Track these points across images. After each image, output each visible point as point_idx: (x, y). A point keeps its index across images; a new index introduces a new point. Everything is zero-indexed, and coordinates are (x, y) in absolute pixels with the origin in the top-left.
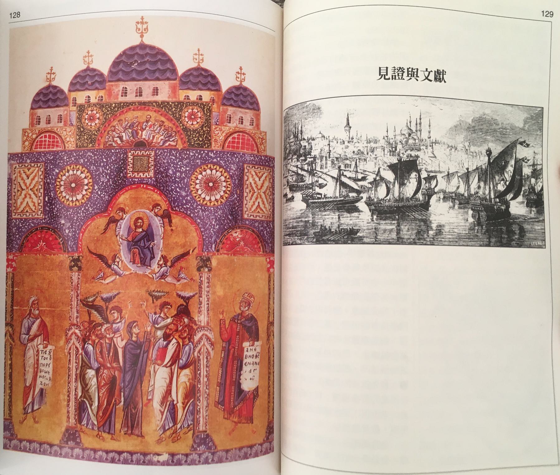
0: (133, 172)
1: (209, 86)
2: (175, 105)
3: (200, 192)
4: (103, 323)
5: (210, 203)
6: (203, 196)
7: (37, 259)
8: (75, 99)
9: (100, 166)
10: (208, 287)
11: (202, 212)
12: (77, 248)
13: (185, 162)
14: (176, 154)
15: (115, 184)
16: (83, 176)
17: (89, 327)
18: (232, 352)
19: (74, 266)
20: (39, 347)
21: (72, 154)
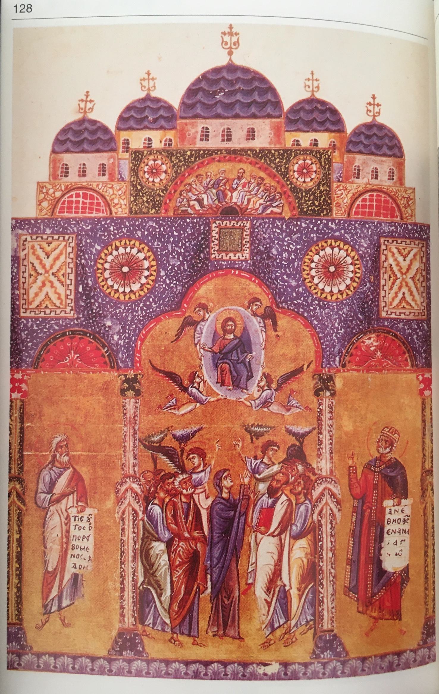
0: (219, 251)
1: (328, 125)
2: (279, 153)
3: (316, 281)
4: (176, 472)
5: (332, 296)
6: (321, 286)
7: (64, 379)
8: (127, 142)
9: (169, 241)
10: (331, 419)
11: (320, 309)
12: (133, 362)
13: (294, 237)
14: (282, 225)
15: (193, 268)
16: (141, 256)
17: (154, 479)
18: (367, 514)
19: (128, 389)
20: (69, 511)
21: (122, 223)
